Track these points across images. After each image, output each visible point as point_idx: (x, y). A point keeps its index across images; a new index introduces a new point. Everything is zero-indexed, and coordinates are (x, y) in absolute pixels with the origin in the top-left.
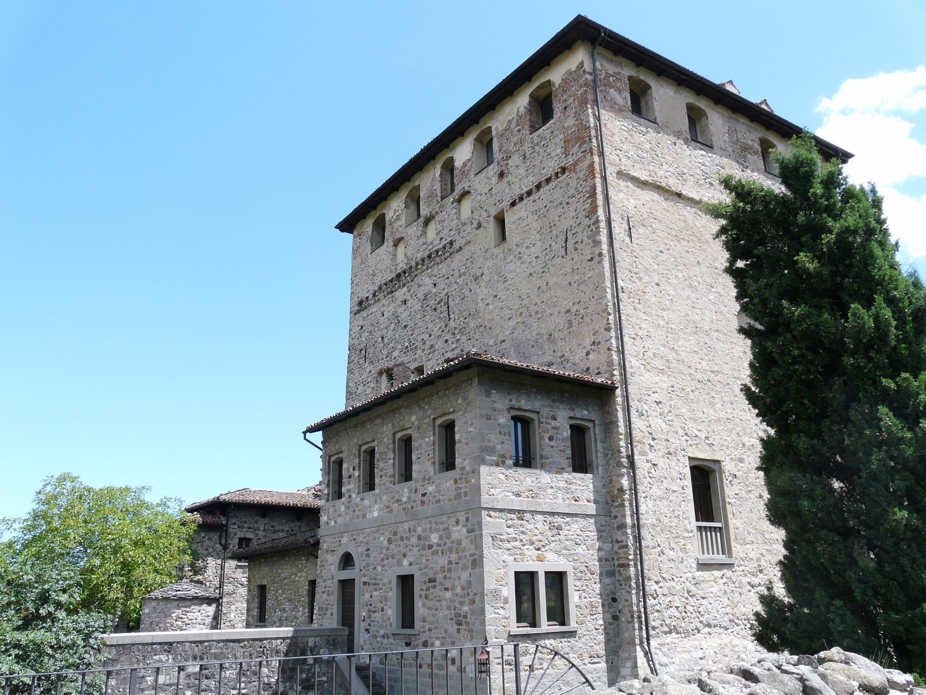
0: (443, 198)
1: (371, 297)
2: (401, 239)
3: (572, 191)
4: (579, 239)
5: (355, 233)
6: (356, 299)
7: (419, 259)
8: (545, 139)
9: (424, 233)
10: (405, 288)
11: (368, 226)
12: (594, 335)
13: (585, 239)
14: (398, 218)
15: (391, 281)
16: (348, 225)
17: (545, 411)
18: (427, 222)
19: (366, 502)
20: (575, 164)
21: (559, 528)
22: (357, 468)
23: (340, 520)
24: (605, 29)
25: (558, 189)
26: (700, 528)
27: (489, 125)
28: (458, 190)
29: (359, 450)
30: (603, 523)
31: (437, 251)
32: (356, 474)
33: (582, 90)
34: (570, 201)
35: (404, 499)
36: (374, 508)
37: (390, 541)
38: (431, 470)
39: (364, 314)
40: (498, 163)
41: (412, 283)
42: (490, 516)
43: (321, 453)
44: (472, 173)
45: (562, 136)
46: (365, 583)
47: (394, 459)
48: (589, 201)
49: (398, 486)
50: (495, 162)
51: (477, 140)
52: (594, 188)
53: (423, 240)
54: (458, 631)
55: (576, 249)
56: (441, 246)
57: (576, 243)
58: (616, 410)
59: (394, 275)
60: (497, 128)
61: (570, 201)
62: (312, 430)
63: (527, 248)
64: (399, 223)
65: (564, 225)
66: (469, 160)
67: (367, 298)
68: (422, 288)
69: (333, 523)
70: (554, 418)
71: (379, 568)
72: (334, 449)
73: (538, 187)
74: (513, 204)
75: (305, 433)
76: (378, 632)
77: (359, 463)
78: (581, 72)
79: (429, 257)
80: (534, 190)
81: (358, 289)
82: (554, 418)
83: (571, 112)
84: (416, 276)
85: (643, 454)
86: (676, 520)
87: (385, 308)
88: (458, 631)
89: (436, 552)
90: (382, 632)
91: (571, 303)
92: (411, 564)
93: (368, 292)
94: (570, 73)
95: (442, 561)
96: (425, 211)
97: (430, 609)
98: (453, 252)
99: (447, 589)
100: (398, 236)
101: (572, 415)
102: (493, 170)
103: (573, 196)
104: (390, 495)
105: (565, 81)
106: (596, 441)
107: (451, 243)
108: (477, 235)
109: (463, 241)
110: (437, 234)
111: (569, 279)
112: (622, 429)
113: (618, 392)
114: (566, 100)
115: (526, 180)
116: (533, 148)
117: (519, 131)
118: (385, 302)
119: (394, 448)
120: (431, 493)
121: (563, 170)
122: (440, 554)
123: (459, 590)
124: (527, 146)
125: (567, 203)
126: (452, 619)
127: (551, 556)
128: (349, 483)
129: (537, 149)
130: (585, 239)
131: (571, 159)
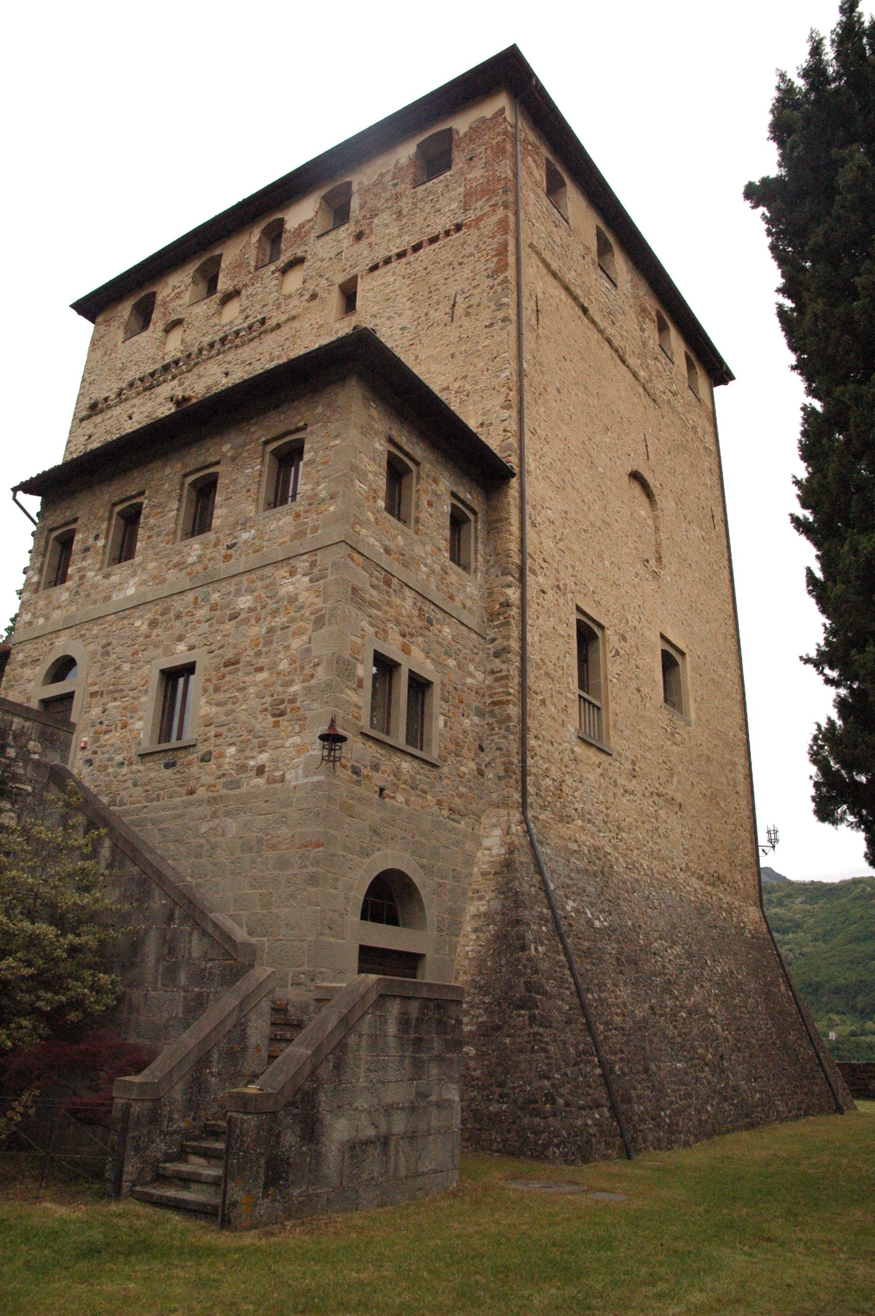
0: (257, 269)
1: (113, 396)
2: (179, 322)
3: (469, 250)
4: (474, 301)
5: (100, 319)
6: (87, 402)
7: (205, 344)
8: (435, 193)
9: (219, 313)
10: (175, 382)
11: (125, 310)
12: (484, 414)
13: (484, 301)
14: (178, 296)
15: (152, 375)
16: (90, 307)
17: (426, 467)
18: (228, 298)
19: (115, 579)
20: (479, 219)
21: (430, 621)
22: (103, 536)
23: (57, 615)
24: (538, 81)
25: (448, 248)
26: (580, 697)
27: (348, 179)
28: (284, 259)
29: (111, 512)
30: (477, 645)
31: (237, 333)
32: (101, 543)
33: (500, 138)
34: (465, 260)
35: (190, 560)
36: (129, 584)
37: (153, 624)
38: (250, 509)
39: (98, 419)
40: (357, 222)
41: (189, 375)
42: (352, 560)
43: (34, 528)
44: (313, 235)
45: (461, 190)
46: (93, 695)
47: (178, 510)
48: (495, 260)
49: (179, 545)
50: (352, 222)
51: (324, 198)
52: (505, 245)
53: (216, 320)
54: (276, 724)
55: (468, 314)
56: (245, 325)
57: (470, 307)
58: (508, 503)
59: (158, 366)
60: (361, 183)
61: (465, 260)
62: (29, 487)
63: (389, 318)
64: (180, 302)
65: (452, 289)
66: (309, 221)
67: (106, 399)
68: (204, 379)
69: (41, 621)
70: (436, 481)
71: (126, 667)
72: (58, 517)
73: (417, 248)
74: (374, 268)
75: (15, 490)
76: (111, 759)
77: (108, 529)
78: (500, 119)
79: (223, 340)
80: (409, 251)
81: (93, 388)
82: (436, 481)
83: (480, 163)
84: (196, 364)
85: (534, 573)
86: (560, 672)
87: (135, 409)
88: (276, 724)
89: (247, 621)
90: (119, 758)
91: (451, 379)
92: (192, 648)
93: (111, 390)
94: (484, 120)
95: (257, 630)
96: (224, 284)
97: (218, 704)
98: (265, 332)
99: (260, 669)
100: (174, 317)
101: (454, 490)
102: (345, 232)
103: (472, 255)
104: (165, 560)
105: (474, 130)
106: (476, 538)
107: (263, 321)
108: (307, 308)
109: (284, 317)
110: (242, 311)
111: (452, 349)
112: (515, 529)
113: (514, 482)
114: (473, 149)
115: (398, 241)
116: (414, 204)
117: (395, 185)
118: (137, 401)
119: (181, 495)
120: (245, 542)
121: (458, 227)
122: (253, 621)
123: (284, 665)
124: (405, 204)
125: (460, 264)
126: (266, 710)
127: (417, 653)
128: (84, 559)
129: (421, 205)
130: (484, 301)
131: (472, 215)
